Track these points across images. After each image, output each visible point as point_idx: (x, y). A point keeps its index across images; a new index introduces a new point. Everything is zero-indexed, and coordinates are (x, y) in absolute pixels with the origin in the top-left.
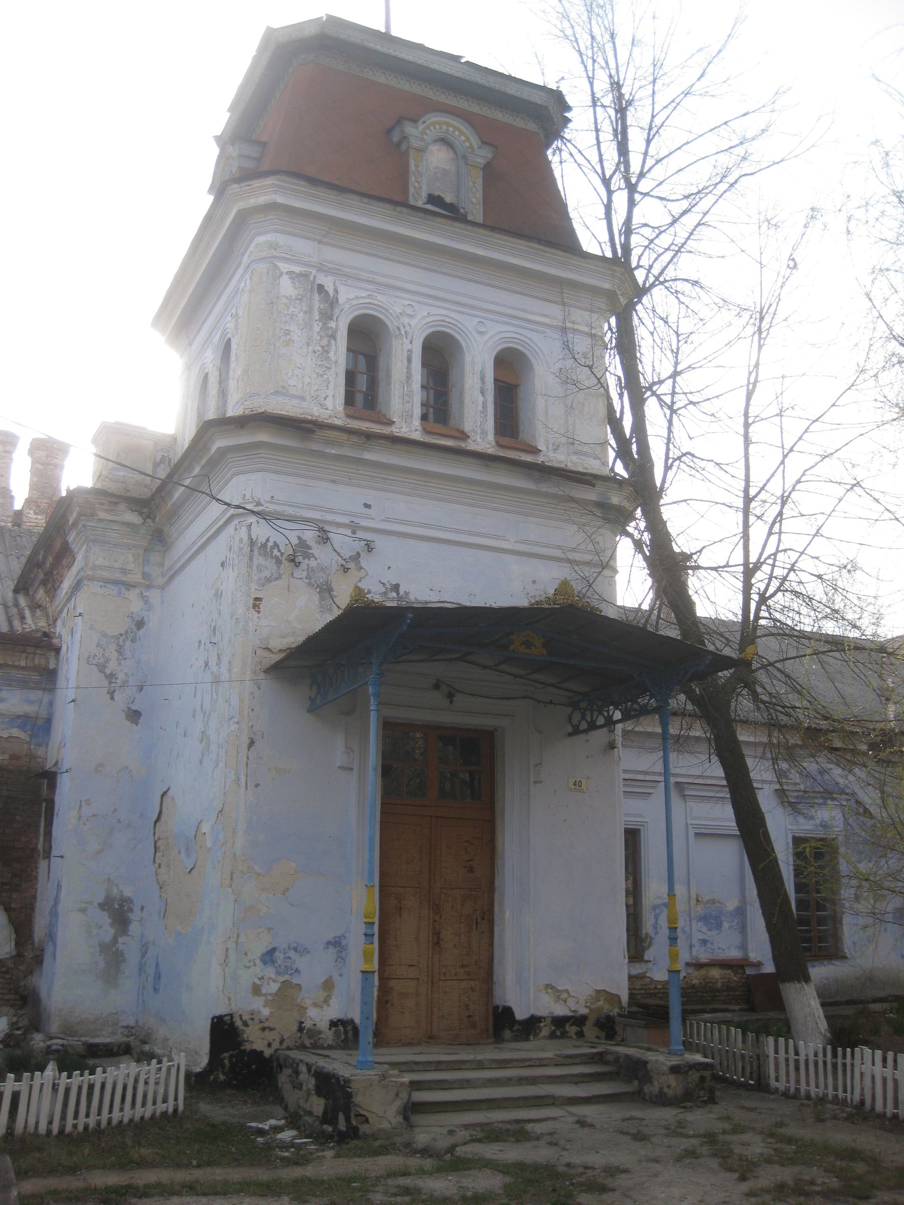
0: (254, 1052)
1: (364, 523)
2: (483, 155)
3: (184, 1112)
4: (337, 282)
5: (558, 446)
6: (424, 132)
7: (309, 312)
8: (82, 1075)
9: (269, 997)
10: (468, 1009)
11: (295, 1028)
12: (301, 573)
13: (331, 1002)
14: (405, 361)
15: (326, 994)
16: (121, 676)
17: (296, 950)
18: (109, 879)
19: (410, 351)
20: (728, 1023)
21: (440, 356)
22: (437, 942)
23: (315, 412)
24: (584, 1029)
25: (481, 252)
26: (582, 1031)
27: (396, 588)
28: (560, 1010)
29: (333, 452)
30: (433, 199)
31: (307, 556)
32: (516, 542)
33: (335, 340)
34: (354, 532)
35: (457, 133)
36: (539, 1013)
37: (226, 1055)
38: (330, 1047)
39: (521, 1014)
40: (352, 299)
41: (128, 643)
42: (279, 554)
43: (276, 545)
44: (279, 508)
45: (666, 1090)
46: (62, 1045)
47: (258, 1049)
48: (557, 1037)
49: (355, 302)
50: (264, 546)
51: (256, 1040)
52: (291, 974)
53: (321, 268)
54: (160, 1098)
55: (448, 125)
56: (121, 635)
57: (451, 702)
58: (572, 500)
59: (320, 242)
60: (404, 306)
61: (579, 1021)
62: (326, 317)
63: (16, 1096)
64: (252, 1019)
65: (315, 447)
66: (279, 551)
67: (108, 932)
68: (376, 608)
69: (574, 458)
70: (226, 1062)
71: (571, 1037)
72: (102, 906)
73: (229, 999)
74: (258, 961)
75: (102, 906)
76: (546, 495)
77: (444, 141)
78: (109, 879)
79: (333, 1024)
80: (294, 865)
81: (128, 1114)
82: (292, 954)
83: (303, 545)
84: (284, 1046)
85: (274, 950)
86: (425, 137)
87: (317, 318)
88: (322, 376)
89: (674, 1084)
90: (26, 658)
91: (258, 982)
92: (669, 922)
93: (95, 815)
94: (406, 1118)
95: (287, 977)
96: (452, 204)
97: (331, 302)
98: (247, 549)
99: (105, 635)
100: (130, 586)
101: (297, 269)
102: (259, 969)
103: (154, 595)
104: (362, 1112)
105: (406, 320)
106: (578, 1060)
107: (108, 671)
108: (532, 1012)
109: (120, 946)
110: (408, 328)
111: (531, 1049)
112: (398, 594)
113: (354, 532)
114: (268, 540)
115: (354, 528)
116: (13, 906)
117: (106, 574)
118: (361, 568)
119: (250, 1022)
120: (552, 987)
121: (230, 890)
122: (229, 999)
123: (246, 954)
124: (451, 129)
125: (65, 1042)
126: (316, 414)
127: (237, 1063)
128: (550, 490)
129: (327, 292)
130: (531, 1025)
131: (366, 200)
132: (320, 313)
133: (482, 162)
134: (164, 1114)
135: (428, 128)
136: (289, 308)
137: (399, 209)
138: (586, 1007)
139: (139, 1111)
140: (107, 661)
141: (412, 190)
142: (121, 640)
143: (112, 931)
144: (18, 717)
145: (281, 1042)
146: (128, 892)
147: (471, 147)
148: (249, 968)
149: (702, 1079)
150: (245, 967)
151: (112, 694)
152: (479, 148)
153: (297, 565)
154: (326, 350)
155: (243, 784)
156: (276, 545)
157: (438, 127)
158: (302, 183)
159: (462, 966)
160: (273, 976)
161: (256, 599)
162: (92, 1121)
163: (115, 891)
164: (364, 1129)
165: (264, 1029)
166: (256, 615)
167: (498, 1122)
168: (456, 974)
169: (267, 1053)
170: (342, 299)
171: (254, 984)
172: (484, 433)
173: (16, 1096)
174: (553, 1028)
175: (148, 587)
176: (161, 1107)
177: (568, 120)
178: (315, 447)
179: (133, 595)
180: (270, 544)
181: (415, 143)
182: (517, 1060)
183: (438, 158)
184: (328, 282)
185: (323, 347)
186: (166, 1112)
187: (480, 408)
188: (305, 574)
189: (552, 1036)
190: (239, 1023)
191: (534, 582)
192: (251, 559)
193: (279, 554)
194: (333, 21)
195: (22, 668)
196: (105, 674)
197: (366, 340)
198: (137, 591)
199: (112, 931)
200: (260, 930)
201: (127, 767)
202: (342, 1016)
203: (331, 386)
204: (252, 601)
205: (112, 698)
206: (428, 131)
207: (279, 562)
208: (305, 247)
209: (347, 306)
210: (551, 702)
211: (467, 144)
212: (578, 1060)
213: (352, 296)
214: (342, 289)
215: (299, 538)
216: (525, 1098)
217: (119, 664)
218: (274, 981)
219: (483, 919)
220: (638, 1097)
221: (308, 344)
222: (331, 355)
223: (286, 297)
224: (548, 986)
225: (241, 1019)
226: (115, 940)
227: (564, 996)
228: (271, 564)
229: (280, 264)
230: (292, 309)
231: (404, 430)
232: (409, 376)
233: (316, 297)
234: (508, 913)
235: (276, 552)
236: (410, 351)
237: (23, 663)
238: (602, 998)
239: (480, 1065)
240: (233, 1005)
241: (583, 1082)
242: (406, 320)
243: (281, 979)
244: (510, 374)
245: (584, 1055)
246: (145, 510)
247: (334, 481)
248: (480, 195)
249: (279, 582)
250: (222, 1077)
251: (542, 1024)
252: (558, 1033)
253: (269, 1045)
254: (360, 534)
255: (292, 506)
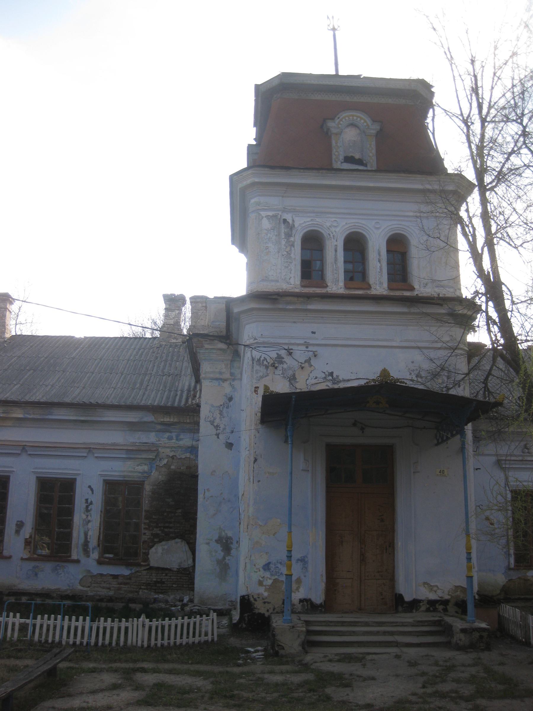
0: (260, 614)
1: (311, 342)
2: (374, 128)
3: (217, 641)
4: (294, 216)
5: (426, 284)
6: (339, 123)
7: (279, 235)
8: (157, 621)
9: (267, 587)
10: (382, 595)
11: (281, 602)
12: (279, 372)
13: (300, 590)
14: (334, 252)
15: (297, 586)
16: (222, 426)
17: (281, 563)
18: (220, 528)
19: (336, 245)
20: (516, 607)
21: (355, 245)
22: (363, 559)
23: (284, 287)
24: (448, 607)
25: (371, 185)
26: (446, 608)
27: (331, 374)
28: (432, 596)
29: (291, 307)
30: (349, 159)
31: (281, 362)
32: (401, 341)
33: (294, 247)
34: (307, 347)
35: (359, 119)
36: (419, 598)
37: (246, 615)
38: (299, 613)
39: (408, 598)
40: (302, 224)
41: (225, 409)
42: (267, 363)
43: (265, 359)
44: (266, 340)
45: (459, 642)
46: (198, 610)
47: (262, 613)
48: (431, 611)
49: (303, 225)
50: (259, 360)
51: (261, 608)
52: (279, 576)
53: (285, 210)
54: (203, 634)
55: (353, 116)
56: (221, 405)
57: (363, 432)
58: (427, 314)
59: (283, 197)
60: (332, 221)
61: (445, 603)
62: (288, 235)
63: (127, 628)
64: (259, 598)
65: (280, 306)
66: (267, 361)
67: (220, 554)
68: (275, 394)
69: (436, 290)
70: (246, 618)
71: (440, 611)
72: (217, 541)
73: (247, 587)
74: (261, 569)
75: (217, 541)
76: (414, 314)
77: (353, 125)
78: (220, 528)
79: (301, 601)
80: (279, 520)
81: (185, 641)
82: (279, 565)
83: (279, 357)
84: (275, 611)
85: (269, 563)
86: (340, 126)
87: (283, 237)
88: (287, 267)
89: (463, 639)
90: (190, 418)
91: (261, 579)
92: (467, 549)
93: (212, 496)
94: (303, 648)
95: (276, 577)
96: (359, 159)
97: (290, 227)
98: (251, 363)
99: (212, 406)
100: (225, 380)
101: (270, 213)
102: (262, 573)
103: (236, 383)
104: (280, 644)
105: (333, 229)
106: (426, 624)
107: (215, 424)
108: (414, 597)
109: (227, 561)
110: (334, 233)
111: (408, 618)
112: (332, 377)
113: (307, 347)
114: (261, 357)
115: (307, 345)
116: (191, 541)
117: (212, 376)
118: (312, 366)
119: (257, 599)
120: (428, 584)
121: (247, 534)
122: (247, 587)
123: (255, 565)
124: (355, 118)
125: (199, 608)
126: (285, 288)
127: (252, 620)
128: (415, 311)
129: (288, 222)
130: (414, 604)
131: (302, 171)
132: (285, 234)
133: (374, 132)
134: (206, 642)
135: (341, 120)
136: (267, 235)
137: (321, 171)
138: (449, 595)
139: (191, 640)
140: (215, 419)
141: (334, 157)
142: (221, 408)
143: (222, 554)
144: (189, 447)
145: (274, 609)
146: (230, 534)
147: (368, 125)
148: (257, 572)
149: (481, 637)
150: (255, 572)
151: (218, 435)
152: (372, 125)
153: (276, 368)
154: (289, 253)
155: (252, 481)
156: (265, 359)
157: (347, 118)
158: (266, 169)
159: (378, 572)
160: (269, 576)
161: (256, 387)
162: (166, 642)
163: (223, 534)
164: (281, 652)
165: (265, 603)
166: (256, 395)
167: (357, 653)
168: (375, 576)
169: (267, 614)
170: (296, 225)
171: (259, 580)
172: (381, 283)
173: (127, 628)
174: (428, 606)
175: (234, 380)
176: (203, 638)
177: (432, 94)
178: (280, 306)
179: (226, 385)
180: (262, 359)
181: (334, 131)
182: (388, 622)
183: (350, 135)
184: (288, 217)
185: (287, 252)
186: (208, 641)
187: (379, 270)
188: (281, 372)
189: (428, 610)
190: (252, 599)
191: (413, 362)
192: (253, 368)
193: (267, 363)
194: (284, 75)
195: (188, 423)
196: (214, 426)
197: (313, 242)
198: (228, 382)
199: (222, 554)
200: (262, 554)
201: (227, 472)
202: (305, 597)
203: (292, 272)
204: (254, 389)
205: (218, 438)
206: (341, 122)
207: (267, 367)
208: (274, 201)
209: (300, 228)
210: (424, 428)
211: (365, 124)
212: (426, 624)
213: (302, 222)
214: (296, 219)
215: (277, 354)
216: (380, 642)
217: (221, 420)
218: (270, 579)
219: (390, 546)
220: (448, 645)
221: (279, 252)
222: (292, 255)
223: (266, 230)
224: (425, 583)
225: (253, 597)
226: (224, 558)
227: (435, 589)
228: (263, 369)
229: (262, 213)
230: (269, 235)
231: (334, 289)
232: (336, 260)
233: (283, 226)
234: (400, 544)
235: (265, 363)
236: (336, 245)
237: (188, 421)
238: (459, 590)
239: (367, 624)
240: (249, 590)
241: (423, 635)
242: (333, 229)
243: (273, 578)
244: (397, 247)
245: (430, 621)
246: (228, 341)
247: (295, 322)
248: (374, 151)
249: (267, 378)
250: (244, 626)
251: (421, 604)
252: (431, 609)
253: (268, 611)
254: (310, 348)
255: (272, 338)
